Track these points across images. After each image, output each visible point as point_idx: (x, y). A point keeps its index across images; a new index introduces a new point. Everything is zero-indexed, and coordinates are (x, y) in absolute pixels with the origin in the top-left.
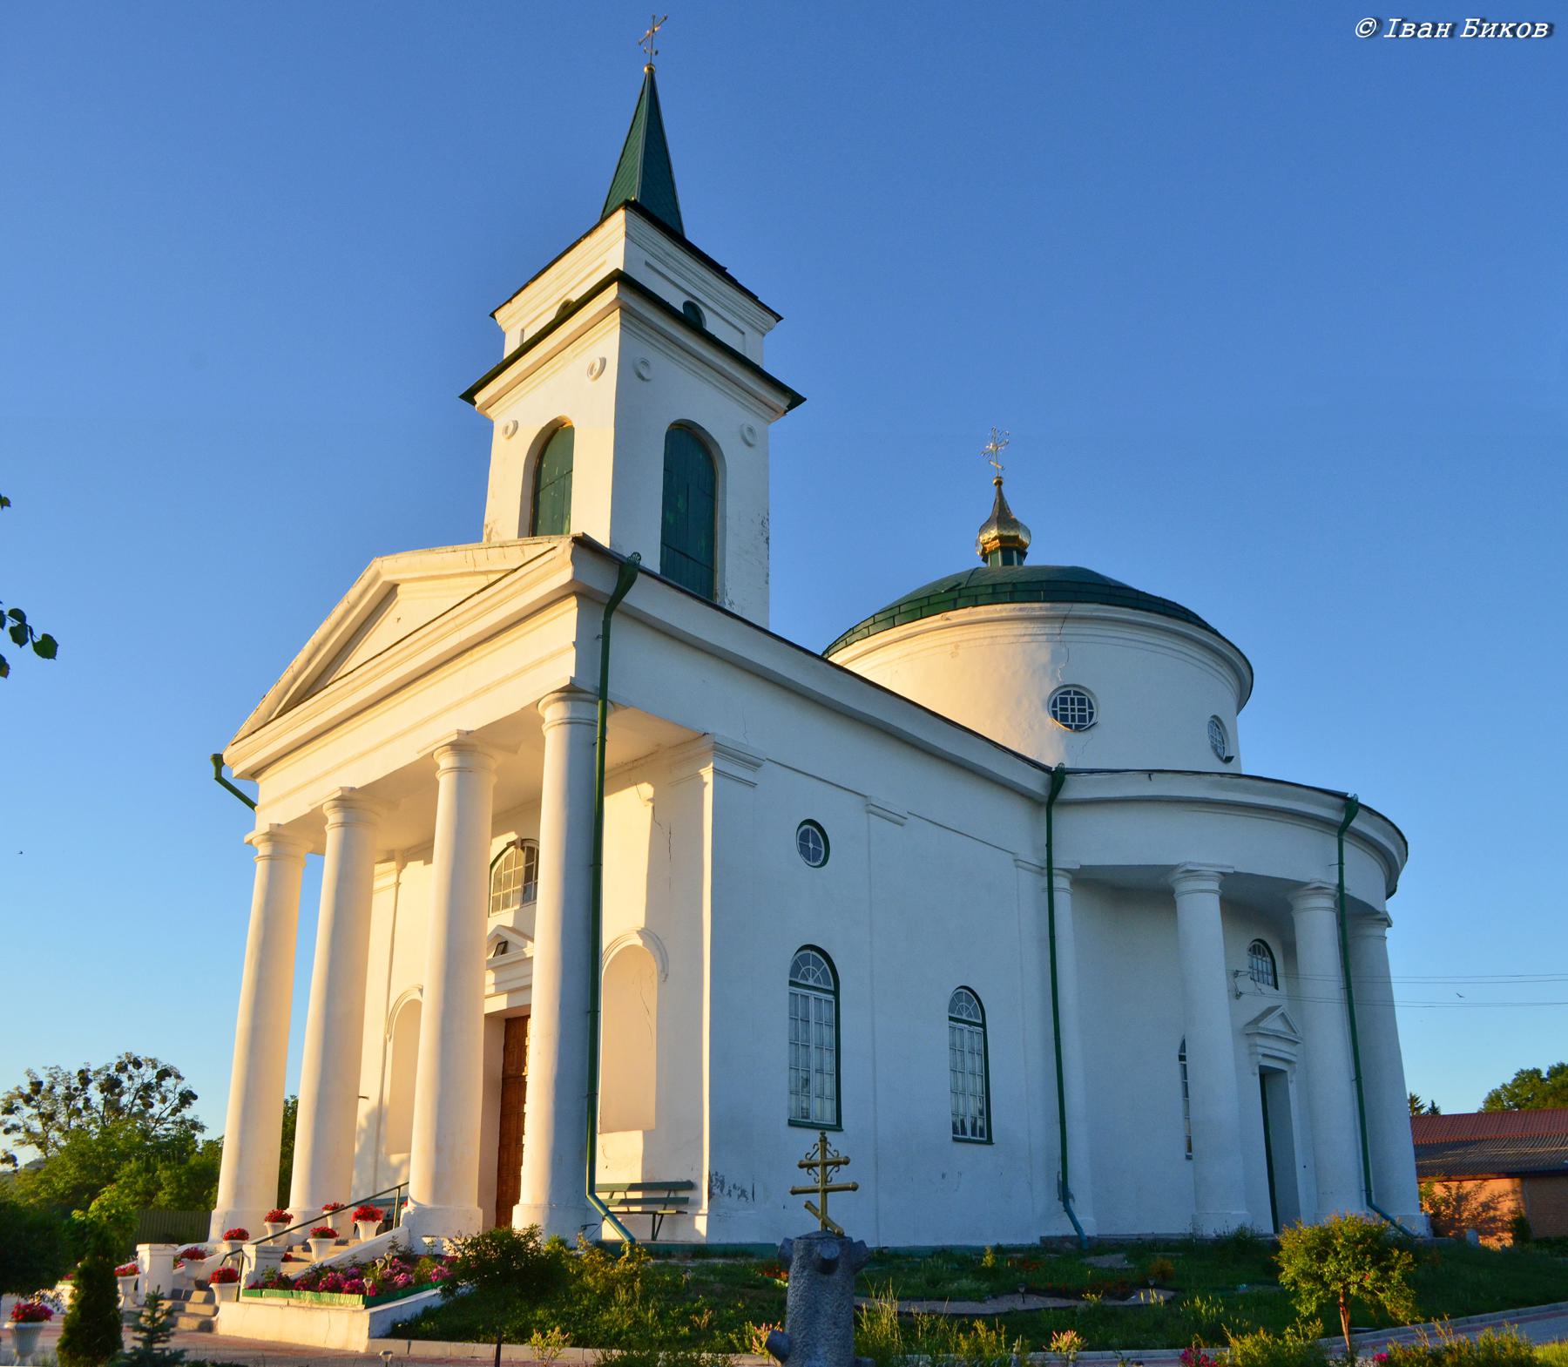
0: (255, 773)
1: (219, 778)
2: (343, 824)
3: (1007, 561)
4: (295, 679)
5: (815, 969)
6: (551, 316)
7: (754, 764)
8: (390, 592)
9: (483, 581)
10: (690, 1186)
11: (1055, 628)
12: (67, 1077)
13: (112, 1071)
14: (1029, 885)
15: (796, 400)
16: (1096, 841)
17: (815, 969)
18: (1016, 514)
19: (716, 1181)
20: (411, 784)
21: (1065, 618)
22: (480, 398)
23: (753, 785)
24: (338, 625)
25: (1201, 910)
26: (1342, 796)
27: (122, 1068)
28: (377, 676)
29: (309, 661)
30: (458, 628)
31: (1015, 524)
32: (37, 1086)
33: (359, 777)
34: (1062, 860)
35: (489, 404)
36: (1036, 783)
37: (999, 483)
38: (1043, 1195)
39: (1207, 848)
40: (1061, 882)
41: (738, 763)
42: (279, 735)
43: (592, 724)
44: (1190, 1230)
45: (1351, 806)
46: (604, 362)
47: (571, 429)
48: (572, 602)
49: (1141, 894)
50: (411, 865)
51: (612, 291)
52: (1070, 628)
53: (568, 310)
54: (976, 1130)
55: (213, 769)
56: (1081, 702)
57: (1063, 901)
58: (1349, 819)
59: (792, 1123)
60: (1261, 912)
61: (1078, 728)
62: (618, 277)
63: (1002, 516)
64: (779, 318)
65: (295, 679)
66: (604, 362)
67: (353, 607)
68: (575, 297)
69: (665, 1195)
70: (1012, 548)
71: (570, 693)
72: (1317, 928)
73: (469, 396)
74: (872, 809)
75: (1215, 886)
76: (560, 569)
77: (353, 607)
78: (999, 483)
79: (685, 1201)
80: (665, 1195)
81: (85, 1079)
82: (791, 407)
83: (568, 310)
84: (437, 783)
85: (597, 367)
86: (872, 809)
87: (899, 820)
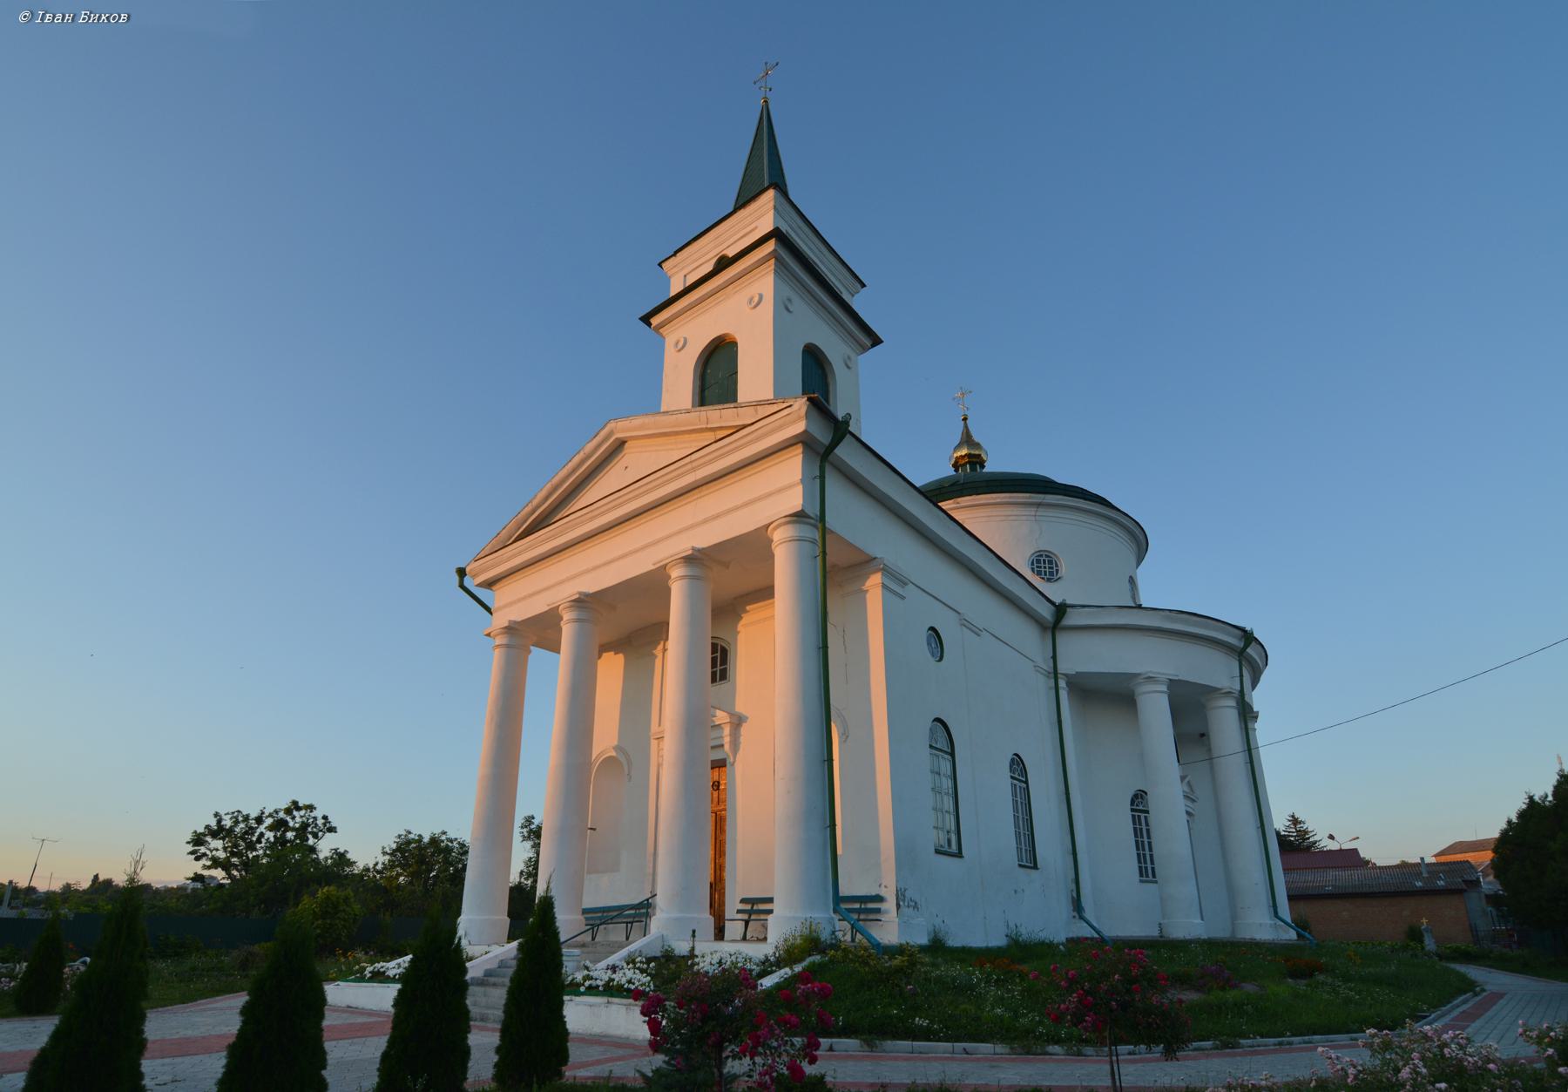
0: (490, 584)
1: (462, 586)
2: (578, 620)
3: (973, 469)
4: (534, 511)
5: (943, 736)
6: (709, 268)
7: (903, 582)
8: (620, 445)
9: (711, 437)
10: (879, 899)
11: (1032, 511)
12: (246, 818)
13: (282, 815)
14: (1042, 684)
15: (876, 341)
16: (1086, 655)
17: (943, 736)
18: (976, 438)
19: (900, 896)
20: (652, 587)
21: (1039, 505)
22: (655, 321)
23: (903, 598)
24: (574, 471)
25: (1156, 710)
26: (1242, 630)
27: (288, 811)
28: (635, 498)
29: (547, 498)
30: (694, 469)
31: (978, 446)
32: (221, 827)
33: (591, 585)
34: (1062, 668)
35: (662, 325)
36: (1046, 612)
37: (965, 419)
38: (1064, 908)
39: (1156, 662)
40: (1062, 683)
41: (896, 581)
42: (520, 553)
43: (813, 542)
44: (1155, 933)
45: (1248, 637)
46: (761, 297)
47: (734, 344)
48: (799, 449)
49: (1108, 696)
50: (605, 655)
51: (770, 246)
52: (1041, 512)
53: (723, 263)
54: (1030, 861)
55: (457, 578)
56: (1050, 562)
57: (1063, 694)
58: (1246, 646)
59: (937, 852)
60: (1190, 708)
61: (1049, 580)
62: (776, 234)
63: (967, 439)
64: (863, 285)
65: (534, 511)
66: (761, 297)
67: (588, 457)
68: (731, 253)
69: (857, 906)
70: (976, 461)
71: (799, 517)
72: (1224, 719)
73: (646, 319)
74: (966, 624)
75: (1164, 688)
76: (794, 422)
77: (588, 457)
78: (965, 419)
79: (878, 911)
80: (857, 906)
81: (259, 820)
82: (873, 346)
83: (723, 263)
84: (669, 590)
85: (756, 299)
86: (966, 624)
87: (977, 632)
